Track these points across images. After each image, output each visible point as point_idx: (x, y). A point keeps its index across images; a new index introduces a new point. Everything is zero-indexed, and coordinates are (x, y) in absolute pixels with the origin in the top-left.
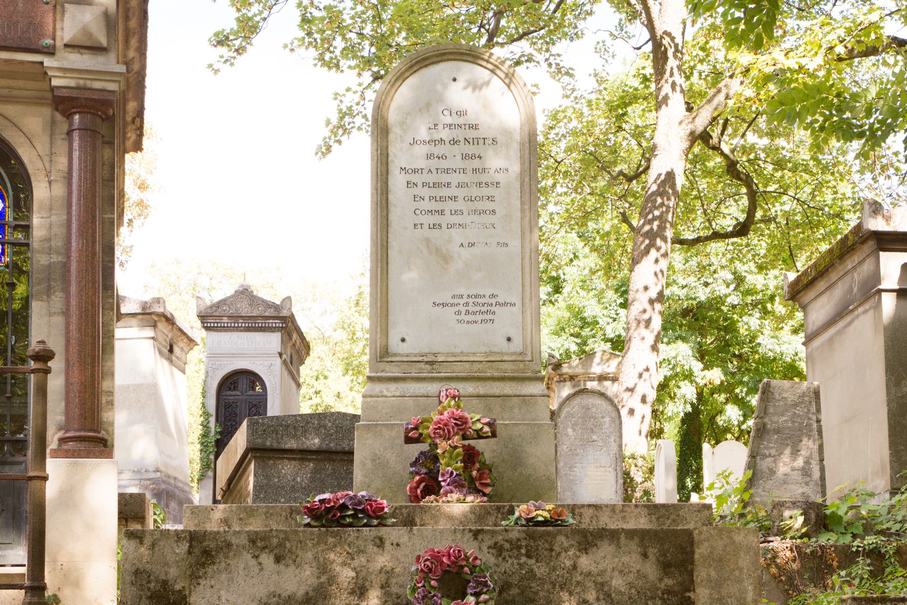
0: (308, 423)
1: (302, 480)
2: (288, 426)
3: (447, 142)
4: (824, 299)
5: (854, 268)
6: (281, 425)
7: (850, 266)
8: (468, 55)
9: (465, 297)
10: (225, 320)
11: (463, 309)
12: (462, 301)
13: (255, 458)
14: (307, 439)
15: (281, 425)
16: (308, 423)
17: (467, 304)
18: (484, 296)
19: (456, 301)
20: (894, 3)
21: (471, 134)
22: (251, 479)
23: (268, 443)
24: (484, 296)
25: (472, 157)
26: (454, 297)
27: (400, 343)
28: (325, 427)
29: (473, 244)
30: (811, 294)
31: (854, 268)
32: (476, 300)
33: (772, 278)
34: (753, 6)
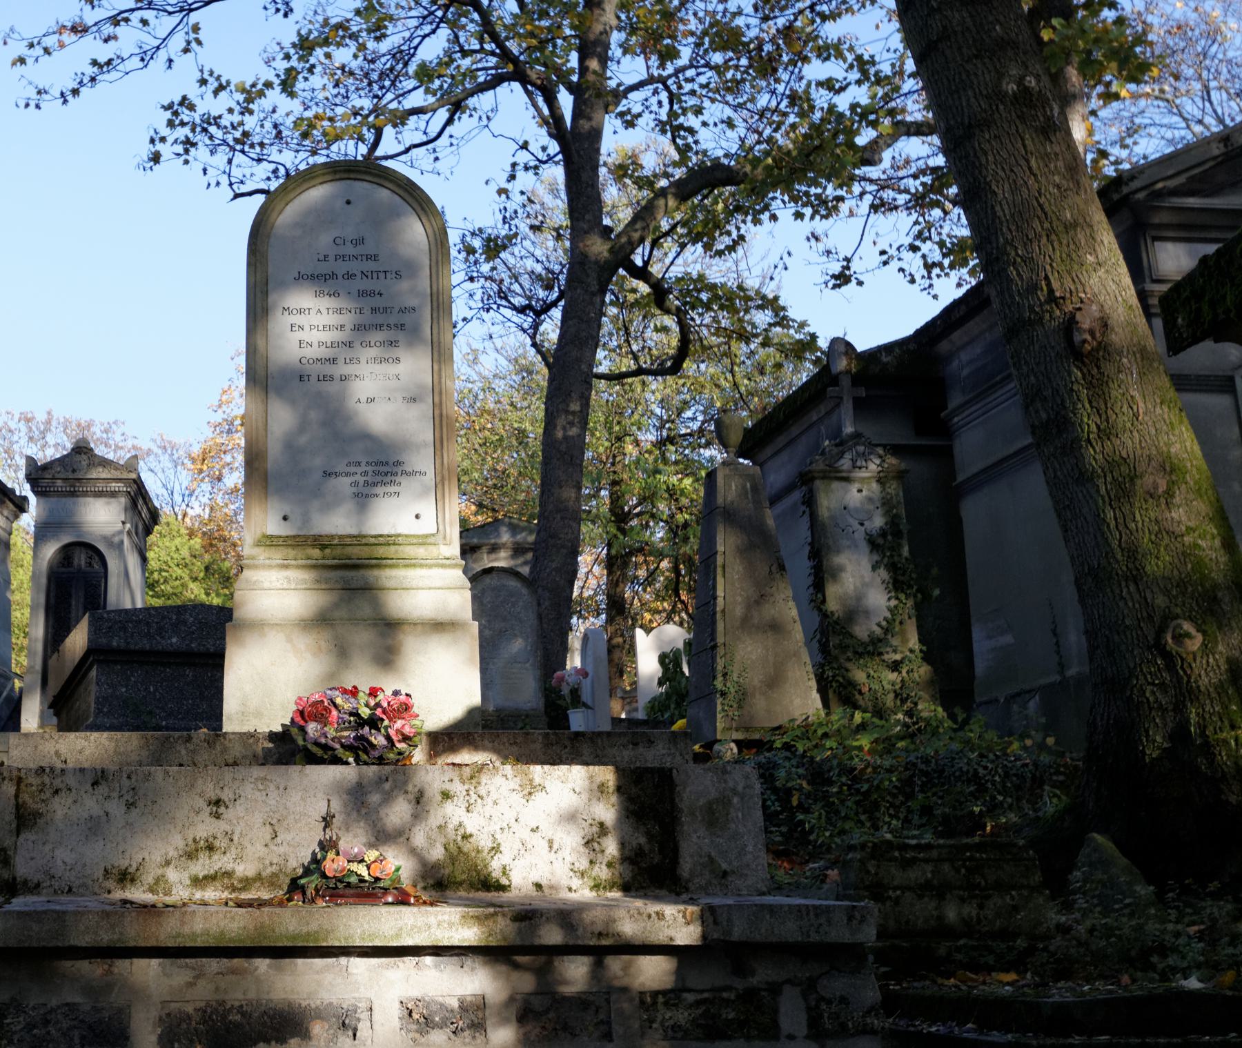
0: (164, 618)
1: (156, 690)
2: (140, 621)
3: (340, 277)
4: (784, 456)
5: (820, 420)
6: (131, 621)
7: (815, 418)
8: (366, 173)
9: (363, 464)
10: (59, 483)
11: (361, 480)
12: (359, 470)
13: (99, 662)
14: (162, 638)
15: (131, 621)
16: (164, 618)
17: (366, 473)
18: (387, 463)
19: (352, 469)
20: (1143, 4)
21: (370, 266)
22: (93, 688)
23: (115, 644)
24: (387, 463)
25: (372, 294)
26: (349, 464)
27: (288, 514)
28: (185, 622)
29: (373, 400)
30: (769, 451)
31: (820, 420)
32: (377, 468)
33: (447, 786)
34: (1080, 42)
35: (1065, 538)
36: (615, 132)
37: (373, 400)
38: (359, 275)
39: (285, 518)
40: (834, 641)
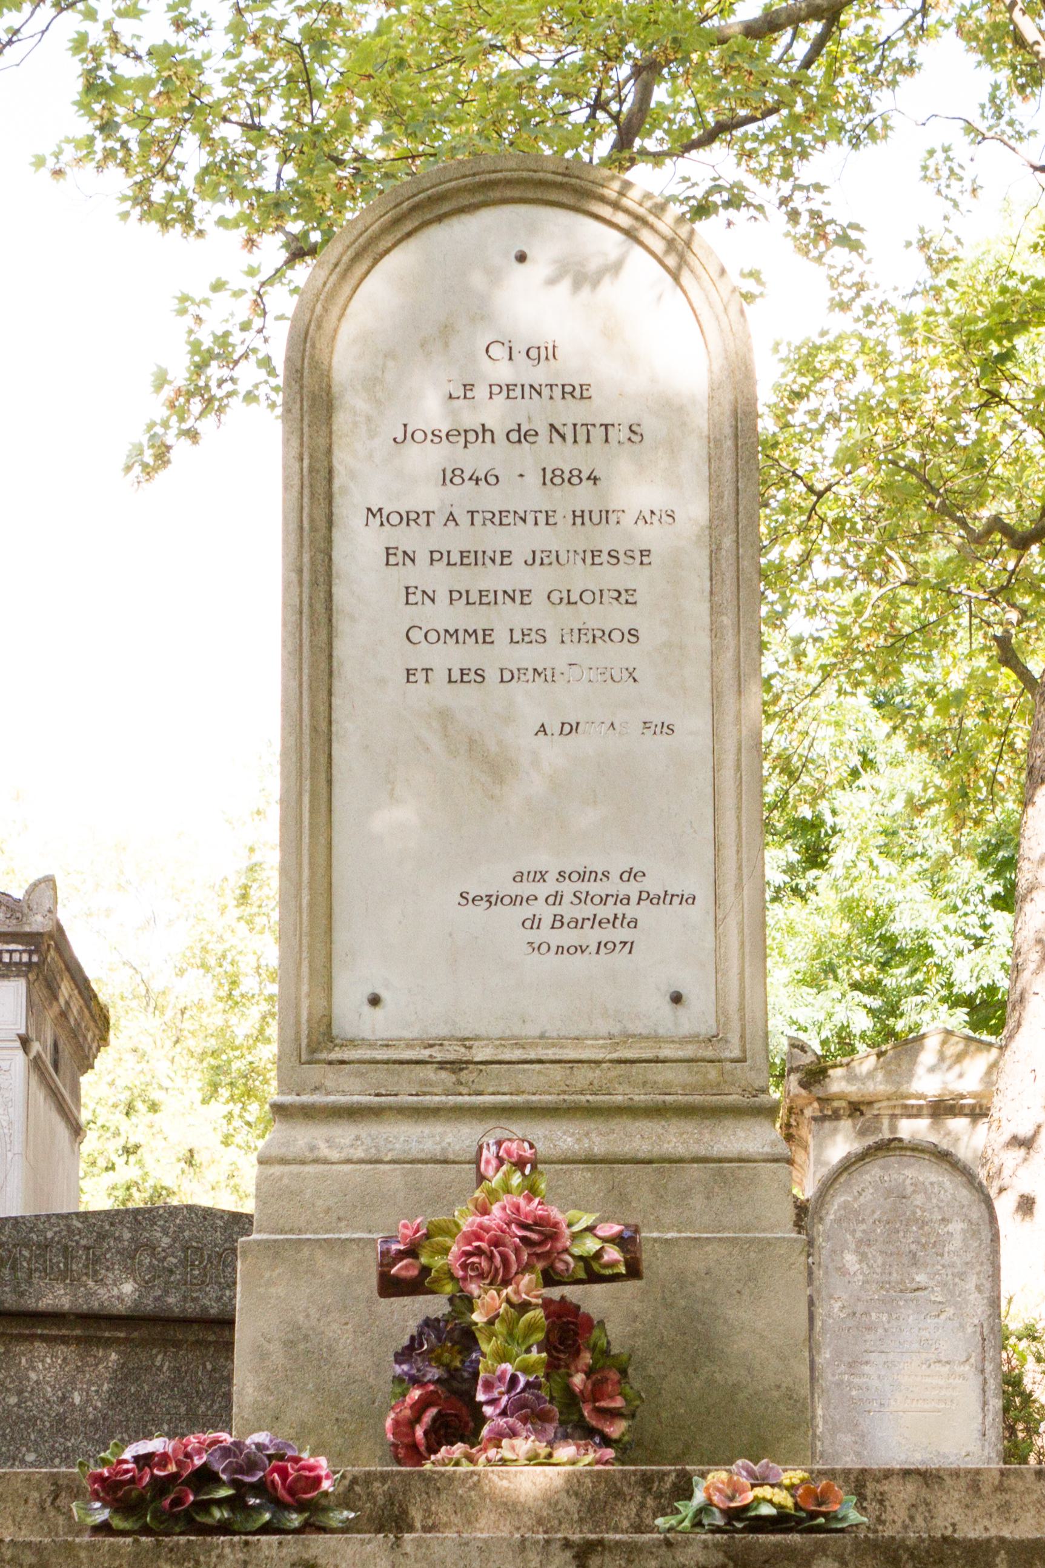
2: (46, 1246)
3: (500, 436)
9: (551, 877)
12: (542, 890)
14: (100, 1282)
16: (102, 1237)
17: (557, 898)
18: (606, 875)
19: (526, 889)
21: (569, 413)
26: (519, 877)
28: (151, 1247)
29: (574, 728)
32: (583, 887)
35: (56, 902)
36: (190, 1159)
37: (574, 728)
38: (544, 431)
39: (521, 258)
40: (977, 1111)
